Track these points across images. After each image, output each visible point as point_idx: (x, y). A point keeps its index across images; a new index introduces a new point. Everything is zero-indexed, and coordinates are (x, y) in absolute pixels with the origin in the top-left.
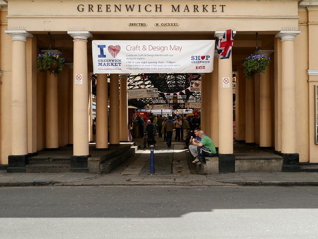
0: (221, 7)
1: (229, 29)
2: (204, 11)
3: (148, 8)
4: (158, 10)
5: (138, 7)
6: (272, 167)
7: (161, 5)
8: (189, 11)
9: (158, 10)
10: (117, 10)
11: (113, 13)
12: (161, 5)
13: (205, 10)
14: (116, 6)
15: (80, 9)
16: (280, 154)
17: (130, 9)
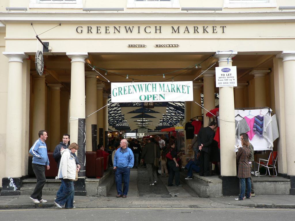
0: (222, 28)
1: (6, 47)
2: (204, 32)
3: (148, 30)
4: (158, 31)
5: (138, 28)
6: (60, 185)
7: (160, 27)
8: (189, 32)
9: (158, 31)
10: (116, 31)
11: (103, 35)
12: (160, 27)
13: (205, 31)
14: (115, 27)
15: (79, 31)
16: (286, 176)
17: (129, 30)
